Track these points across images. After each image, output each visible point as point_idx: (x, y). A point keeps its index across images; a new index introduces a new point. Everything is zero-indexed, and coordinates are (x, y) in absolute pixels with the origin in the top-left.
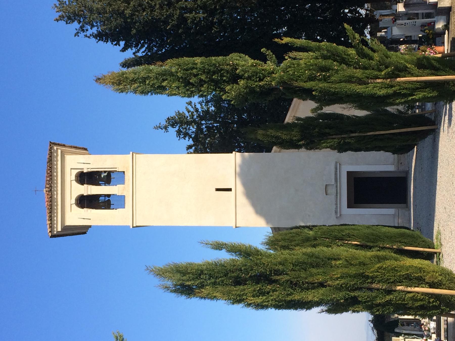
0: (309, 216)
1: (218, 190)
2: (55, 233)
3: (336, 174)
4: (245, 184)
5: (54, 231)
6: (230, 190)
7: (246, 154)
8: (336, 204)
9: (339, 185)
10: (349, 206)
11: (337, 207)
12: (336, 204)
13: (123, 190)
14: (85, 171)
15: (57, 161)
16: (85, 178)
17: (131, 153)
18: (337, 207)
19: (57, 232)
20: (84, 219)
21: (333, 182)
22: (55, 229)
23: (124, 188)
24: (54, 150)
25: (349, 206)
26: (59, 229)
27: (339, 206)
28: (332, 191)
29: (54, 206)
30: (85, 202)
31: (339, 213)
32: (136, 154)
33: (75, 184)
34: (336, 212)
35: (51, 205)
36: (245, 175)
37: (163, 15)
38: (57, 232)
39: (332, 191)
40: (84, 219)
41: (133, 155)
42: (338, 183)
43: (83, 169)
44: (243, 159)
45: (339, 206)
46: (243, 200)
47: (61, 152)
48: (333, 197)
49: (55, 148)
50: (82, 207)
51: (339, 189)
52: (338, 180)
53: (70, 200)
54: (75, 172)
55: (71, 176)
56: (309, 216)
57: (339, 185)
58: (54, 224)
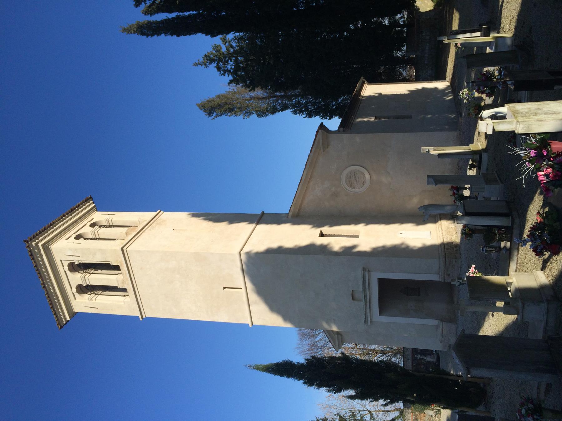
8: (366, 314)
9: (368, 294)
15: (41, 256)
26: (68, 318)
42: (368, 292)
57: (368, 294)
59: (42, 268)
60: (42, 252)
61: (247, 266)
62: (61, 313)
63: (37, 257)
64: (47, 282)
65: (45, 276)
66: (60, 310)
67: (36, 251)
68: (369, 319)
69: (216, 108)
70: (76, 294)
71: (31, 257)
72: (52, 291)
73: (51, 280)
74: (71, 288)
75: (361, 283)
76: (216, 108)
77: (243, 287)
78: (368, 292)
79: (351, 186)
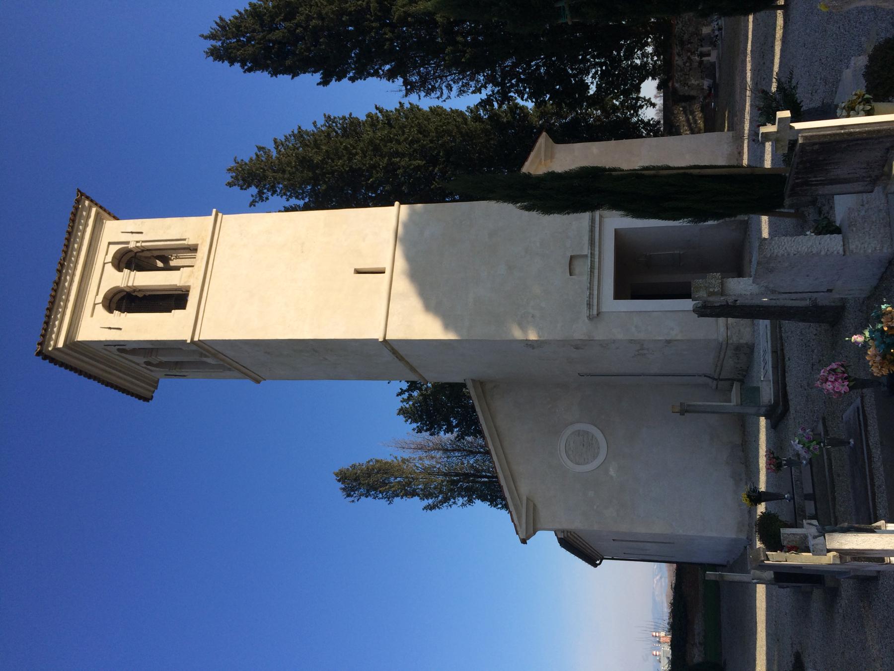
0: (533, 316)
1: (358, 272)
2: (50, 349)
3: (592, 231)
4: (410, 258)
5: (49, 345)
6: (382, 272)
7: (419, 206)
8: (591, 288)
9: (597, 253)
10: (619, 294)
11: (591, 295)
12: (591, 288)
13: (190, 276)
14: (132, 245)
15: (86, 225)
16: (131, 259)
17: (214, 210)
18: (591, 295)
19: (55, 348)
20: (110, 328)
21: (586, 251)
22: (52, 343)
23: (193, 272)
24: (84, 205)
25: (619, 294)
26: (60, 344)
27: (595, 292)
28: (583, 267)
29: (61, 300)
30: (124, 301)
31: (595, 308)
32: (224, 213)
33: (109, 268)
34: (590, 305)
35: (54, 297)
36: (408, 239)
37: (365, 165)
38: (55, 348)
39: (583, 267)
40: (110, 328)
41: (217, 215)
42: (597, 249)
43: (128, 243)
44: (411, 215)
45: (595, 292)
46: (403, 285)
47: (97, 214)
48: (585, 278)
49: (87, 203)
50: (111, 311)
51: (597, 260)
52: (597, 244)
53: (95, 295)
54: (114, 249)
55: (105, 254)
56: (533, 316)
57: (597, 253)
58: (52, 332)
59: (75, 242)
60: (91, 222)
61: (406, 226)
62: (55, 329)
63: (79, 223)
64: (69, 265)
65: (72, 255)
66: (57, 323)
67: (84, 213)
68: (595, 301)
69: (367, 481)
70: (100, 308)
71: (40, 339)
72: (66, 284)
73: (66, 307)
74: (97, 294)
75: (586, 238)
76: (367, 481)
77: (388, 271)
78: (597, 249)
79: (578, 433)
